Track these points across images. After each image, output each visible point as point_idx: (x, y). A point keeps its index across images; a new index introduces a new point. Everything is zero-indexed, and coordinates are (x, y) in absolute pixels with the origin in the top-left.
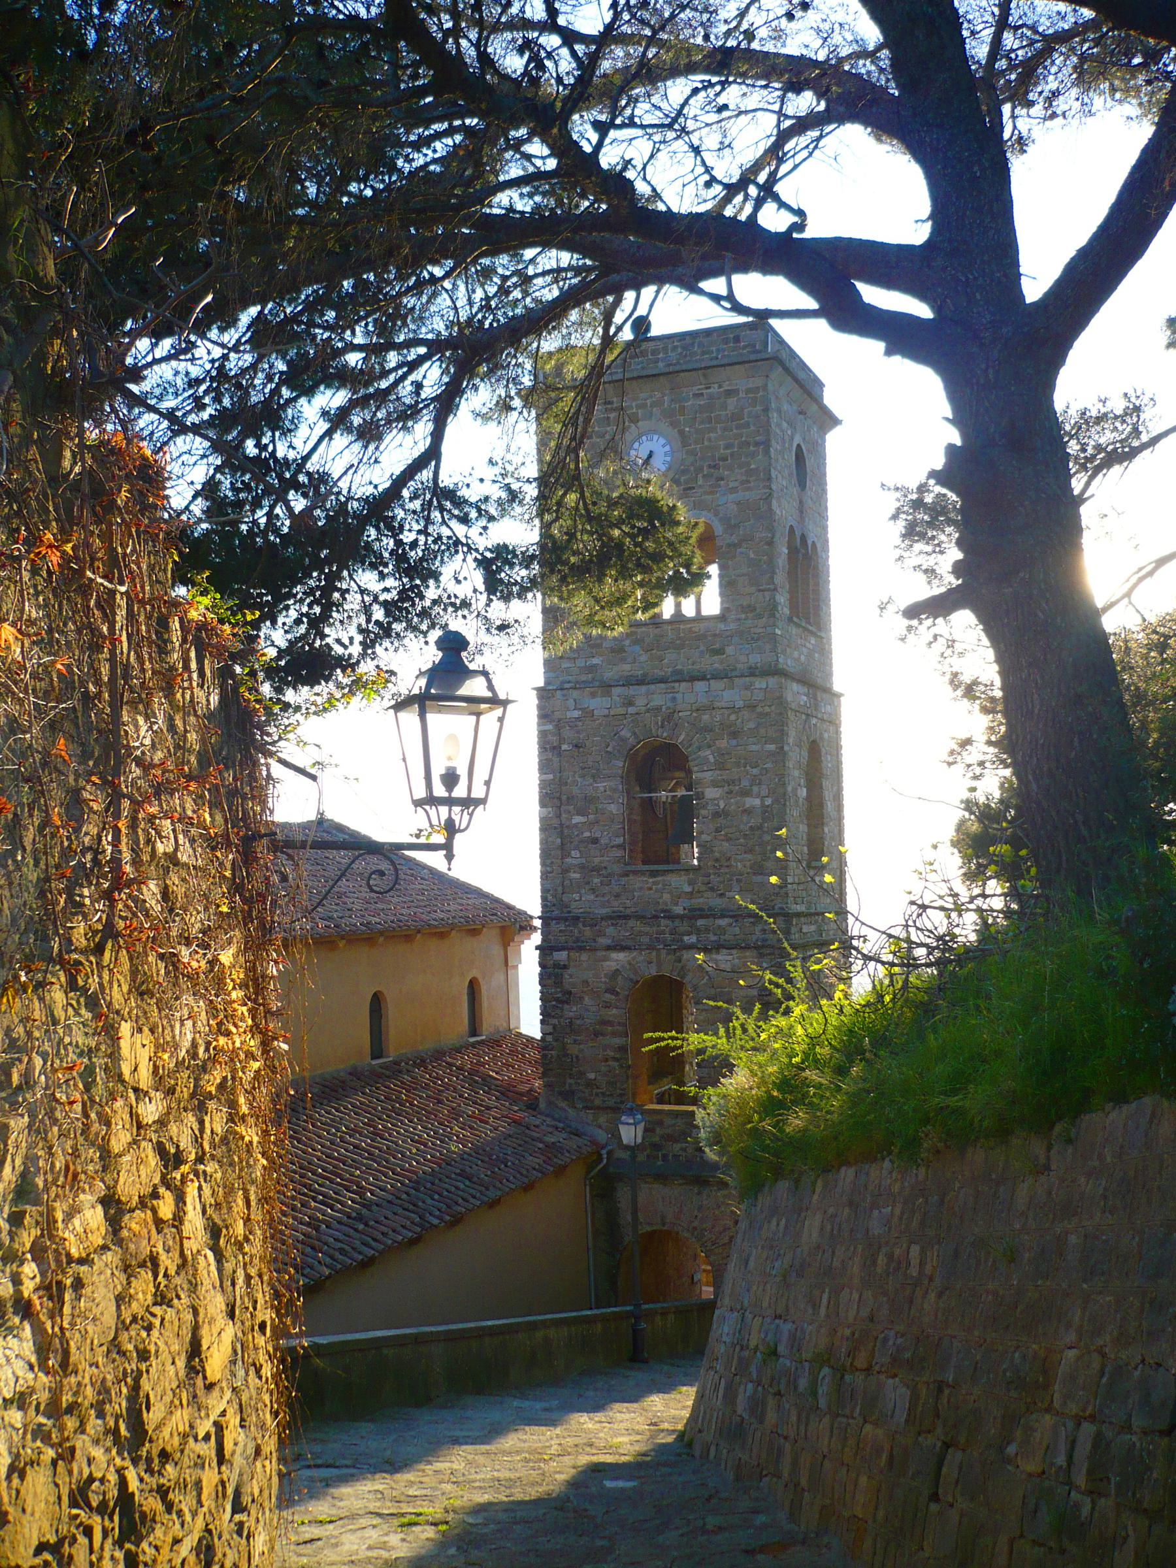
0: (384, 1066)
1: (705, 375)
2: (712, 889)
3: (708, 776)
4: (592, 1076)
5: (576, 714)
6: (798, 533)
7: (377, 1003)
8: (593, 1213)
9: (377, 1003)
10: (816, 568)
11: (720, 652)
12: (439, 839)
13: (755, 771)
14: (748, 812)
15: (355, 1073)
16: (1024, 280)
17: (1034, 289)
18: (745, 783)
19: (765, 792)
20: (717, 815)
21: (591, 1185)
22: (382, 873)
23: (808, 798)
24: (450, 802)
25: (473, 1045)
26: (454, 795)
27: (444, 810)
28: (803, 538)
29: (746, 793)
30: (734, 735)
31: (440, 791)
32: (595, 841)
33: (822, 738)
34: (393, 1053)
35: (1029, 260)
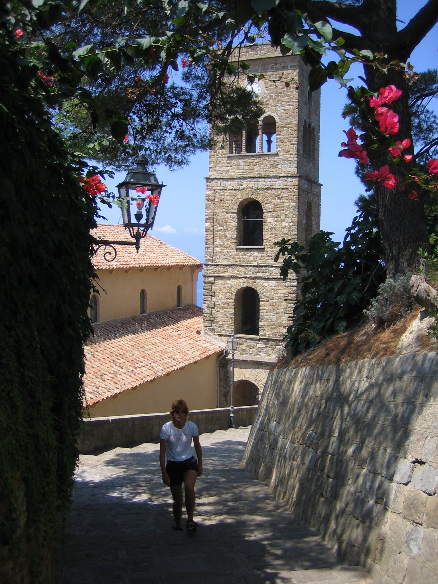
0: (144, 317)
1: (275, 60)
2: (269, 256)
3: (269, 214)
4: (221, 323)
5: (221, 188)
6: (307, 123)
7: (143, 294)
8: (220, 373)
9: (143, 294)
10: (314, 136)
11: (276, 167)
12: (134, 240)
13: (287, 213)
14: (284, 228)
15: (134, 319)
16: (397, 22)
17: (400, 27)
18: (283, 216)
19: (290, 220)
20: (272, 228)
21: (220, 363)
22: (110, 253)
23: (307, 223)
24: (139, 225)
25: (178, 310)
26: (140, 223)
27: (136, 229)
28: (310, 125)
29: (283, 221)
30: (280, 199)
31: (134, 221)
32: (226, 236)
33: (313, 200)
34: (148, 311)
35: (400, 15)
